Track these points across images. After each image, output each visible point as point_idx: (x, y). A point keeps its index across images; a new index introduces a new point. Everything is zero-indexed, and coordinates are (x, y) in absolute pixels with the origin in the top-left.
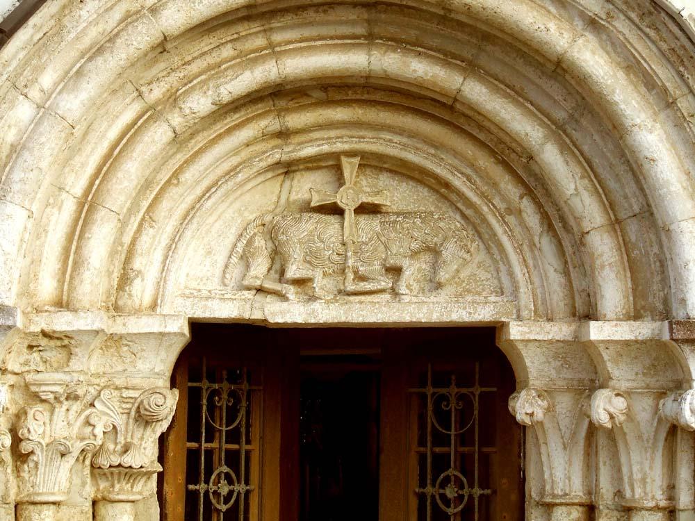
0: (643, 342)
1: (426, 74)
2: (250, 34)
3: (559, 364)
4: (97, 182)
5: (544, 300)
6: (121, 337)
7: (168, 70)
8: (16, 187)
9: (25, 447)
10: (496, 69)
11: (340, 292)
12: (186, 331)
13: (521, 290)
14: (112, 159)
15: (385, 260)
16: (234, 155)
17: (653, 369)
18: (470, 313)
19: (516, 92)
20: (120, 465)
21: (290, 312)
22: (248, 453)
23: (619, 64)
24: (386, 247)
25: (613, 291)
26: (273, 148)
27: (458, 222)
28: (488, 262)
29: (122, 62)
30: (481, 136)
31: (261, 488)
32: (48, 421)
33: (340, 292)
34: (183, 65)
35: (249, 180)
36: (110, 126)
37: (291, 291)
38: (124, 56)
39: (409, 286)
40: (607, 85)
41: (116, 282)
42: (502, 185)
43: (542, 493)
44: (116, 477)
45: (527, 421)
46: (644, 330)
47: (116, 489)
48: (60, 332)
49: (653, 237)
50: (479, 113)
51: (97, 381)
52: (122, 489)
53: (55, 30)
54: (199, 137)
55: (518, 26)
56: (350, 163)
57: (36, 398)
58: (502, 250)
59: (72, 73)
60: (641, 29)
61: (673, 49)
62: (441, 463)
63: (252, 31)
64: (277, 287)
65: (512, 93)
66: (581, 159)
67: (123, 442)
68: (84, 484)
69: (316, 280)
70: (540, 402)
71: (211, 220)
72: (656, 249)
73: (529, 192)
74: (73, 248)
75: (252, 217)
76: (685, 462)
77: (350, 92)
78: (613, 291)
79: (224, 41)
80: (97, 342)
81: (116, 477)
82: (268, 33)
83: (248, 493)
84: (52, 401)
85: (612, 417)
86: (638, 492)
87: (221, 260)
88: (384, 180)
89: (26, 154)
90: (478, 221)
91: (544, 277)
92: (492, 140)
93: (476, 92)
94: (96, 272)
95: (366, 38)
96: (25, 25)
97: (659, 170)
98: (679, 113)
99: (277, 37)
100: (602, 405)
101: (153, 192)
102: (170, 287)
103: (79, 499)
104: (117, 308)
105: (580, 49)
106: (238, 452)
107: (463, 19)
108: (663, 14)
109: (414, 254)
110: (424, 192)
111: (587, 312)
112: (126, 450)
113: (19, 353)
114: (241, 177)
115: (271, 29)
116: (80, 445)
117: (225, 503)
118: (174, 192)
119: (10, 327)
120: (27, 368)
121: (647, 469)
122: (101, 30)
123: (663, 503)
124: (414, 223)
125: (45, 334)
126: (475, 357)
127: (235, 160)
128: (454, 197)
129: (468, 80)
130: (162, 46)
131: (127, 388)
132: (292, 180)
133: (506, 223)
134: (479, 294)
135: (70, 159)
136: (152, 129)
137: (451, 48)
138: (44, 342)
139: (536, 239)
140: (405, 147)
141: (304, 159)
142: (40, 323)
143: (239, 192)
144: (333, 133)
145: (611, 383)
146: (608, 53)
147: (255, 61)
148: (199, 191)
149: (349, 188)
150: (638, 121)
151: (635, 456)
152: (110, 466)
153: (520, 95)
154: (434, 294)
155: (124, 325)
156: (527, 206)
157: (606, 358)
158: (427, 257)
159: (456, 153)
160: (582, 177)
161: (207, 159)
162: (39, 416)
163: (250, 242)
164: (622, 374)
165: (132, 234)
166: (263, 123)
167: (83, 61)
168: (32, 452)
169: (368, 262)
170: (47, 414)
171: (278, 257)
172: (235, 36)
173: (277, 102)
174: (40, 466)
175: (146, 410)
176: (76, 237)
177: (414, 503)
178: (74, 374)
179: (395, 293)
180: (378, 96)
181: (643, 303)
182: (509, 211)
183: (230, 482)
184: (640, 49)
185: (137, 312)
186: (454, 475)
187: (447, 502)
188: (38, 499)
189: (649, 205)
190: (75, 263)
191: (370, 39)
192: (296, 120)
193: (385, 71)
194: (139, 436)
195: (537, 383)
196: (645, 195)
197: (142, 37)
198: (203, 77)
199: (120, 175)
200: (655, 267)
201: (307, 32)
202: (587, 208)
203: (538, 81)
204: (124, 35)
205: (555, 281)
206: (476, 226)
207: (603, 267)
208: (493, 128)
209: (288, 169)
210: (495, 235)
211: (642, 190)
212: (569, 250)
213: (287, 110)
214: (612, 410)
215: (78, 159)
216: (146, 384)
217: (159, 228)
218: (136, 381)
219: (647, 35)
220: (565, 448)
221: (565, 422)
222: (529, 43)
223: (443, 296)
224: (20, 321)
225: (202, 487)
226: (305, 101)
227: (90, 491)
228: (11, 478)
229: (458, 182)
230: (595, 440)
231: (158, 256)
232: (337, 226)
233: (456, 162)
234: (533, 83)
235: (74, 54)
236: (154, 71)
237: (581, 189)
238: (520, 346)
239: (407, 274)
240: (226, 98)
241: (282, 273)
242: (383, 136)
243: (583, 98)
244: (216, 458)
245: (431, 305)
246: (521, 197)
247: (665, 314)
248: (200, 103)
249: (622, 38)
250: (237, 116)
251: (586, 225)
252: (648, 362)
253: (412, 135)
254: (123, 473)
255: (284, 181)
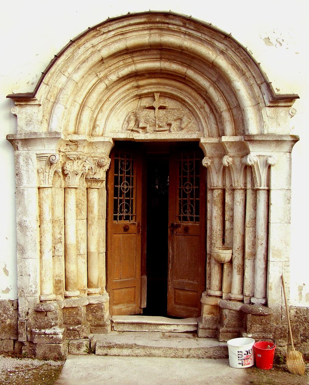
0: (237, 142)
1: (176, 68)
2: (127, 58)
3: (215, 150)
4: (85, 99)
5: (211, 132)
6: (93, 143)
7: (105, 68)
8: (61, 99)
9: (66, 172)
10: (196, 66)
11: (154, 131)
12: (112, 141)
13: (205, 129)
14: (89, 93)
15: (167, 122)
16: (124, 93)
17: (240, 150)
18: (190, 136)
19: (202, 73)
20: (93, 178)
21: (140, 136)
22: (133, 178)
23: (229, 63)
24: (167, 118)
25: (229, 128)
26: (135, 91)
27: (187, 111)
28: (196, 122)
29: (90, 65)
30: (193, 86)
31: (136, 187)
32: (72, 165)
33: (154, 131)
34: (109, 67)
35: (128, 100)
36: (89, 84)
37: (140, 131)
38: (91, 63)
39: (173, 129)
40: (226, 69)
41: (92, 128)
42: (199, 100)
43: (211, 186)
44: (92, 182)
45: (206, 165)
46: (237, 138)
47: (93, 185)
48: (75, 140)
49: (240, 113)
50: (192, 80)
51: (87, 155)
52: (94, 185)
53: (72, 56)
54: (114, 88)
55: (201, 53)
56: (157, 95)
57: (69, 159)
58: (199, 118)
59: (76, 68)
60: (235, 53)
61: (244, 59)
62: (185, 180)
63: (128, 57)
64: (137, 129)
65: (201, 73)
66: (220, 92)
67: (94, 172)
68: (83, 183)
69: (147, 127)
70: (209, 160)
71: (119, 111)
72: (241, 116)
73: (207, 102)
74: (79, 117)
75: (130, 111)
76: (249, 175)
77: (156, 75)
78: (229, 128)
79: (120, 60)
80: (85, 144)
81: (92, 182)
82: (133, 58)
83: (132, 189)
84: (73, 160)
85: (228, 163)
86: (236, 184)
87: (122, 122)
88: (167, 100)
89: (64, 91)
90: (193, 111)
91: (211, 126)
92: (196, 87)
93: (191, 73)
94: (85, 124)
95: (160, 59)
96: (63, 55)
97: (241, 93)
98: (246, 77)
99: (135, 59)
100: (225, 160)
101: (101, 103)
102: (107, 129)
103: (82, 187)
104: (92, 135)
105: (218, 59)
106: (130, 177)
107: (186, 52)
108: (241, 49)
109: (175, 120)
110: (178, 103)
111: (221, 133)
112: (95, 173)
113: (64, 147)
114: (126, 99)
115: (133, 56)
116: (82, 172)
117: (126, 191)
118: (107, 103)
119: (59, 138)
120: (66, 151)
121: (238, 178)
122: (85, 56)
123: (243, 188)
124: (175, 111)
125: (70, 141)
126: (193, 149)
127: (125, 94)
128: (186, 104)
129: (188, 70)
130: (102, 60)
131: (95, 157)
132: (141, 100)
133: (201, 111)
134: (194, 131)
135: (78, 93)
136: (100, 84)
137: (184, 61)
138: (70, 143)
139: (209, 115)
140: (172, 90)
141: (144, 94)
142: (69, 138)
143: (126, 103)
144: (152, 86)
145: (228, 154)
146: (226, 60)
147: (129, 65)
148: (115, 103)
149: (157, 102)
150: (235, 79)
151: (235, 175)
152: (90, 178)
153: (203, 74)
154: (181, 131)
155: (93, 139)
156: (206, 106)
157: (227, 146)
158: (179, 121)
159: (186, 92)
160: (220, 96)
161: (117, 94)
162: (69, 164)
163: (129, 117)
164: (231, 151)
165: (96, 115)
166: (132, 84)
167: (79, 65)
168: (68, 174)
169: (162, 122)
170: (72, 164)
171: (137, 121)
172: (123, 59)
173: (136, 78)
174: (70, 178)
175: (100, 163)
176: (79, 115)
177: (178, 191)
178: (79, 152)
179: (170, 131)
180: (164, 76)
181: (238, 132)
182: (201, 107)
183: (127, 185)
184: (235, 59)
185: (98, 136)
186: (189, 183)
187: (186, 190)
188: (70, 187)
189: (239, 104)
190: (79, 122)
191: (161, 59)
192: (141, 83)
193: (165, 68)
194: (99, 170)
195: (208, 155)
196: (238, 101)
197: (96, 58)
198: (114, 70)
199: (91, 97)
200: (241, 121)
201: (143, 58)
202: (222, 105)
203: (207, 70)
204: (91, 58)
205: (214, 126)
206: (192, 112)
207: (226, 121)
208: (197, 84)
209: (140, 97)
210: (198, 114)
211: (237, 100)
212: (218, 118)
213: (139, 80)
214: (228, 161)
215: (80, 93)
216: (100, 156)
217: (104, 113)
218: (97, 155)
219: (237, 55)
220: (217, 173)
221: (217, 166)
222: (204, 58)
223: (183, 132)
224: (62, 137)
225: (119, 186)
226: (143, 77)
227: (85, 185)
228: (63, 181)
229: (187, 100)
230: (225, 170)
231: (104, 121)
232: (153, 112)
233: (187, 94)
234: (207, 71)
235: (77, 63)
236: (101, 68)
237: (220, 99)
238: (204, 145)
239: (173, 125)
240: (121, 76)
241: (138, 126)
242: (166, 87)
243: (220, 74)
244: (123, 179)
245: (180, 134)
246: (204, 104)
247: (244, 134)
248: (114, 77)
249: (230, 56)
250: (125, 82)
251: (222, 110)
252: (238, 148)
253: (174, 87)
254: (94, 181)
255: (139, 100)
